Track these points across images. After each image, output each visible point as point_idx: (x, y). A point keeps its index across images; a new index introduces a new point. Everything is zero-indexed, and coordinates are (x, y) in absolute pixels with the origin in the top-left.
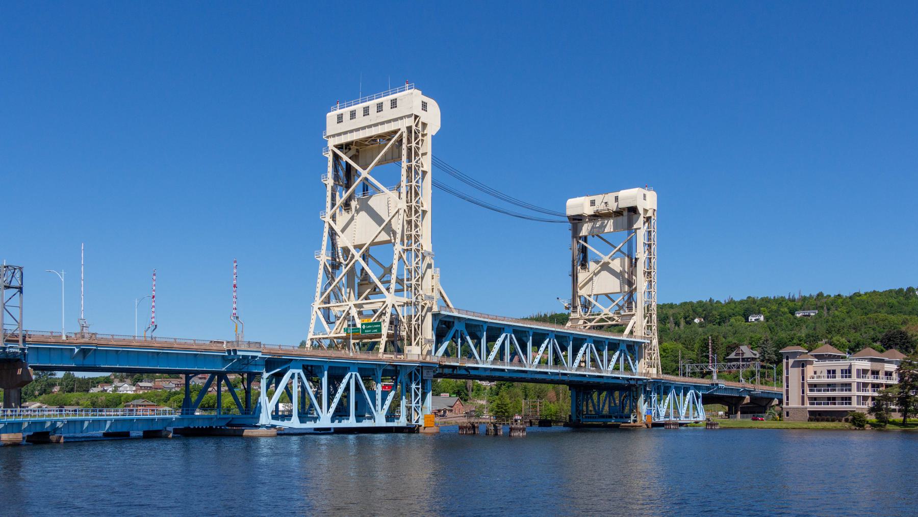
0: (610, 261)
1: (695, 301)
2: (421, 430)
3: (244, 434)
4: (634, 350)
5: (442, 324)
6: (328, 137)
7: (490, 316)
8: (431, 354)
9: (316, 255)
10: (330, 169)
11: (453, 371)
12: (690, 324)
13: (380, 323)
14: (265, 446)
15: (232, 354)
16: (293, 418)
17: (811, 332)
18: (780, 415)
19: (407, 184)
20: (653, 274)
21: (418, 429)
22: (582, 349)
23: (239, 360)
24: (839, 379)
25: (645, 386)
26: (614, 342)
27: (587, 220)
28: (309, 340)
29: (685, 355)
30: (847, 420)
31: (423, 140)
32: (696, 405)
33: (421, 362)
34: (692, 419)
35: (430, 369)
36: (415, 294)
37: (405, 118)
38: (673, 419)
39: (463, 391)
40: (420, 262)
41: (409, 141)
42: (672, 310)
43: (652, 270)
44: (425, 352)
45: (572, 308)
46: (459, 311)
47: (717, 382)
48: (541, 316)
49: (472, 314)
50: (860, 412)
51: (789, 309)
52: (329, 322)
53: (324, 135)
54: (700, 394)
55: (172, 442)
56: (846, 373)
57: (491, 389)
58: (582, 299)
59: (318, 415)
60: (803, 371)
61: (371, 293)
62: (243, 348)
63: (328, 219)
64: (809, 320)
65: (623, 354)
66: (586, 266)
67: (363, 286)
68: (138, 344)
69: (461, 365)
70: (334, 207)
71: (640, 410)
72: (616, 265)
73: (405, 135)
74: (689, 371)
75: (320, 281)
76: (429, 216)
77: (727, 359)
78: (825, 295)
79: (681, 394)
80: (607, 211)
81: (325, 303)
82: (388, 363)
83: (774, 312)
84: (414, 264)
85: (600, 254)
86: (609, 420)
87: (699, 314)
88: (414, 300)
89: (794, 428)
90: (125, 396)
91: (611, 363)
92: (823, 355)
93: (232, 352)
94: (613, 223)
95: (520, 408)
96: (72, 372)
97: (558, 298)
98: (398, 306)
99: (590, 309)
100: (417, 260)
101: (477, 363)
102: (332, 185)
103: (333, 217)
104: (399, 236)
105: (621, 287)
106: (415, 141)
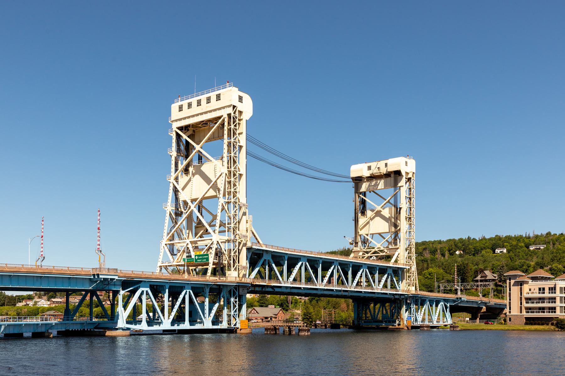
0: (381, 210)
1: (457, 238)
2: (238, 331)
3: (106, 334)
4: (398, 273)
5: (254, 256)
6: (172, 121)
7: (290, 250)
8: (245, 277)
9: (164, 206)
10: (174, 144)
11: (262, 289)
12: (453, 255)
13: (208, 255)
14: (121, 342)
15: (96, 277)
16: (142, 323)
17: (540, 260)
18: (505, 321)
19: (228, 155)
20: (412, 219)
21: (236, 331)
22: (359, 273)
23: (101, 281)
24: (547, 295)
25: (406, 300)
26: (383, 268)
27: (365, 180)
28: (159, 267)
29: (445, 277)
30: (552, 324)
31: (239, 124)
32: (445, 313)
33: (238, 283)
34: (442, 323)
35: (245, 287)
36: (234, 234)
37: (226, 108)
38: (428, 323)
39: (285, 303)
40: (237, 211)
41: (229, 124)
42: (440, 245)
43: (412, 216)
44: (241, 276)
45: (354, 244)
46: (266, 245)
47: (461, 296)
48: (345, 249)
49: (277, 248)
50: (562, 318)
51: (525, 244)
52: (173, 254)
53: (170, 120)
54: (448, 305)
55: (54, 341)
56: (552, 290)
57: (305, 302)
58: (362, 237)
59: (161, 320)
60: (521, 289)
61: (204, 233)
62: (104, 273)
63: (172, 180)
64: (539, 252)
65: (390, 277)
66: (365, 213)
67: (198, 228)
68: (26, 270)
69: (268, 284)
70: (177, 171)
71: (403, 317)
72: (386, 212)
73: (226, 120)
74: (443, 288)
75: (166, 225)
76: (244, 178)
77: (475, 280)
78: (552, 234)
79: (434, 306)
80: (380, 174)
81: (170, 240)
82: (213, 283)
83: (514, 246)
84: (232, 212)
85: (375, 205)
86: (380, 324)
87: (460, 248)
88: (232, 238)
89: (514, 330)
90: (41, 309)
91: (381, 283)
92: (537, 277)
93: (96, 276)
94: (384, 182)
95: (320, 316)
96: (3, 292)
97: (345, 237)
98: (222, 242)
99: (367, 244)
100: (235, 209)
101: (280, 283)
102: (176, 156)
103: (176, 179)
104: (222, 192)
105: (389, 229)
106: (233, 124)
